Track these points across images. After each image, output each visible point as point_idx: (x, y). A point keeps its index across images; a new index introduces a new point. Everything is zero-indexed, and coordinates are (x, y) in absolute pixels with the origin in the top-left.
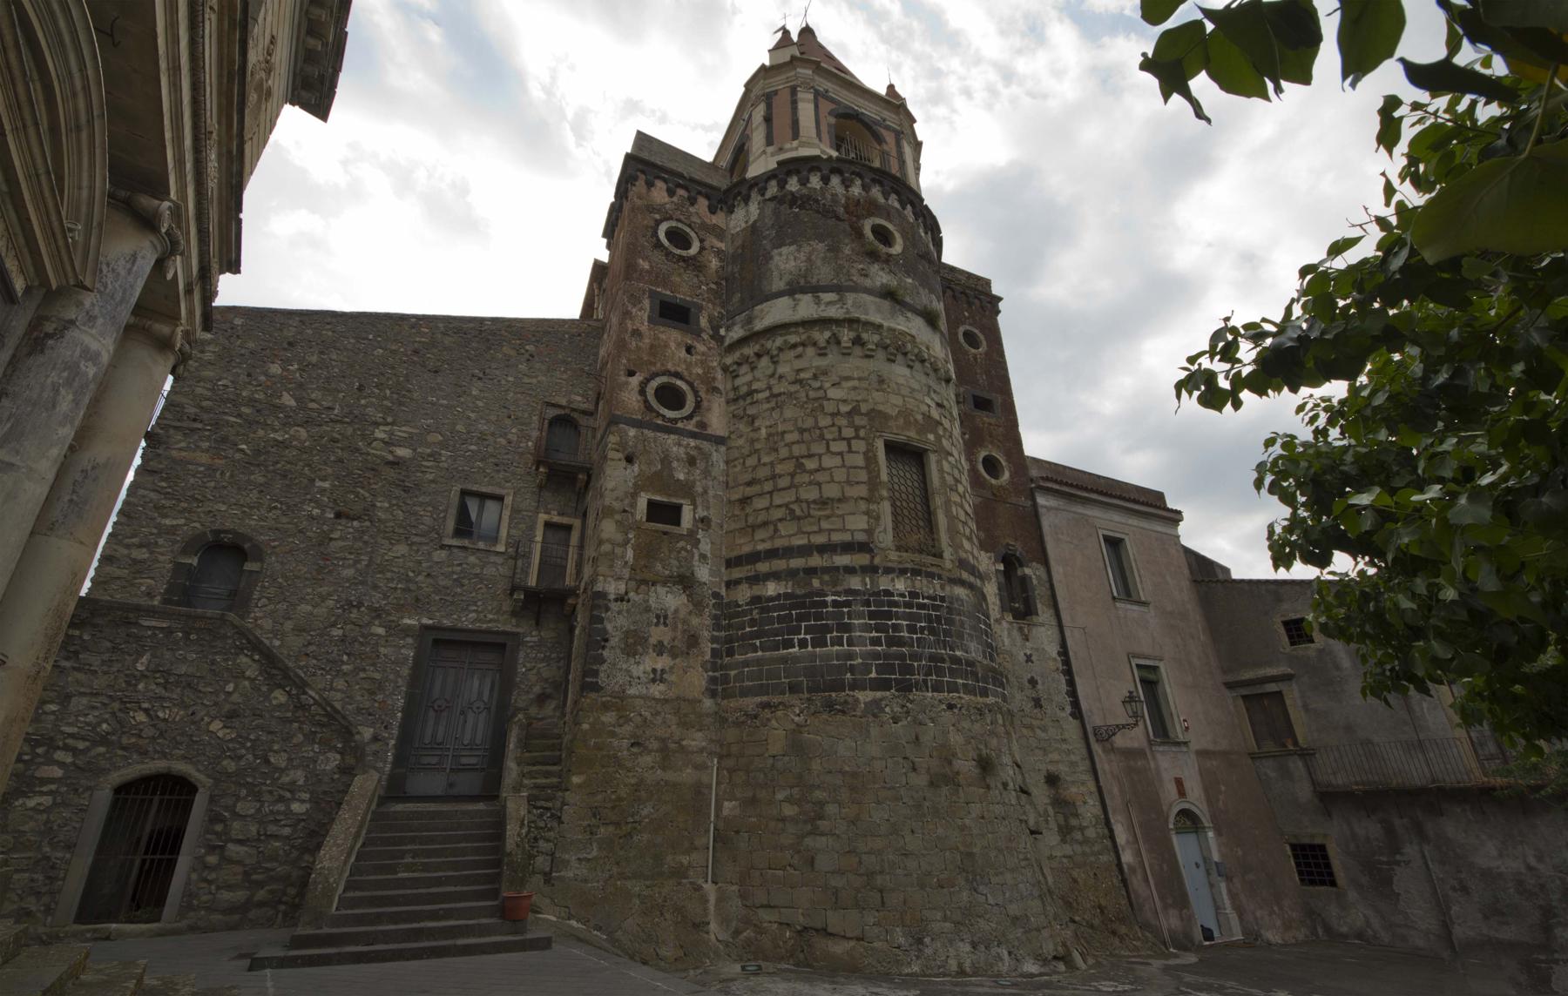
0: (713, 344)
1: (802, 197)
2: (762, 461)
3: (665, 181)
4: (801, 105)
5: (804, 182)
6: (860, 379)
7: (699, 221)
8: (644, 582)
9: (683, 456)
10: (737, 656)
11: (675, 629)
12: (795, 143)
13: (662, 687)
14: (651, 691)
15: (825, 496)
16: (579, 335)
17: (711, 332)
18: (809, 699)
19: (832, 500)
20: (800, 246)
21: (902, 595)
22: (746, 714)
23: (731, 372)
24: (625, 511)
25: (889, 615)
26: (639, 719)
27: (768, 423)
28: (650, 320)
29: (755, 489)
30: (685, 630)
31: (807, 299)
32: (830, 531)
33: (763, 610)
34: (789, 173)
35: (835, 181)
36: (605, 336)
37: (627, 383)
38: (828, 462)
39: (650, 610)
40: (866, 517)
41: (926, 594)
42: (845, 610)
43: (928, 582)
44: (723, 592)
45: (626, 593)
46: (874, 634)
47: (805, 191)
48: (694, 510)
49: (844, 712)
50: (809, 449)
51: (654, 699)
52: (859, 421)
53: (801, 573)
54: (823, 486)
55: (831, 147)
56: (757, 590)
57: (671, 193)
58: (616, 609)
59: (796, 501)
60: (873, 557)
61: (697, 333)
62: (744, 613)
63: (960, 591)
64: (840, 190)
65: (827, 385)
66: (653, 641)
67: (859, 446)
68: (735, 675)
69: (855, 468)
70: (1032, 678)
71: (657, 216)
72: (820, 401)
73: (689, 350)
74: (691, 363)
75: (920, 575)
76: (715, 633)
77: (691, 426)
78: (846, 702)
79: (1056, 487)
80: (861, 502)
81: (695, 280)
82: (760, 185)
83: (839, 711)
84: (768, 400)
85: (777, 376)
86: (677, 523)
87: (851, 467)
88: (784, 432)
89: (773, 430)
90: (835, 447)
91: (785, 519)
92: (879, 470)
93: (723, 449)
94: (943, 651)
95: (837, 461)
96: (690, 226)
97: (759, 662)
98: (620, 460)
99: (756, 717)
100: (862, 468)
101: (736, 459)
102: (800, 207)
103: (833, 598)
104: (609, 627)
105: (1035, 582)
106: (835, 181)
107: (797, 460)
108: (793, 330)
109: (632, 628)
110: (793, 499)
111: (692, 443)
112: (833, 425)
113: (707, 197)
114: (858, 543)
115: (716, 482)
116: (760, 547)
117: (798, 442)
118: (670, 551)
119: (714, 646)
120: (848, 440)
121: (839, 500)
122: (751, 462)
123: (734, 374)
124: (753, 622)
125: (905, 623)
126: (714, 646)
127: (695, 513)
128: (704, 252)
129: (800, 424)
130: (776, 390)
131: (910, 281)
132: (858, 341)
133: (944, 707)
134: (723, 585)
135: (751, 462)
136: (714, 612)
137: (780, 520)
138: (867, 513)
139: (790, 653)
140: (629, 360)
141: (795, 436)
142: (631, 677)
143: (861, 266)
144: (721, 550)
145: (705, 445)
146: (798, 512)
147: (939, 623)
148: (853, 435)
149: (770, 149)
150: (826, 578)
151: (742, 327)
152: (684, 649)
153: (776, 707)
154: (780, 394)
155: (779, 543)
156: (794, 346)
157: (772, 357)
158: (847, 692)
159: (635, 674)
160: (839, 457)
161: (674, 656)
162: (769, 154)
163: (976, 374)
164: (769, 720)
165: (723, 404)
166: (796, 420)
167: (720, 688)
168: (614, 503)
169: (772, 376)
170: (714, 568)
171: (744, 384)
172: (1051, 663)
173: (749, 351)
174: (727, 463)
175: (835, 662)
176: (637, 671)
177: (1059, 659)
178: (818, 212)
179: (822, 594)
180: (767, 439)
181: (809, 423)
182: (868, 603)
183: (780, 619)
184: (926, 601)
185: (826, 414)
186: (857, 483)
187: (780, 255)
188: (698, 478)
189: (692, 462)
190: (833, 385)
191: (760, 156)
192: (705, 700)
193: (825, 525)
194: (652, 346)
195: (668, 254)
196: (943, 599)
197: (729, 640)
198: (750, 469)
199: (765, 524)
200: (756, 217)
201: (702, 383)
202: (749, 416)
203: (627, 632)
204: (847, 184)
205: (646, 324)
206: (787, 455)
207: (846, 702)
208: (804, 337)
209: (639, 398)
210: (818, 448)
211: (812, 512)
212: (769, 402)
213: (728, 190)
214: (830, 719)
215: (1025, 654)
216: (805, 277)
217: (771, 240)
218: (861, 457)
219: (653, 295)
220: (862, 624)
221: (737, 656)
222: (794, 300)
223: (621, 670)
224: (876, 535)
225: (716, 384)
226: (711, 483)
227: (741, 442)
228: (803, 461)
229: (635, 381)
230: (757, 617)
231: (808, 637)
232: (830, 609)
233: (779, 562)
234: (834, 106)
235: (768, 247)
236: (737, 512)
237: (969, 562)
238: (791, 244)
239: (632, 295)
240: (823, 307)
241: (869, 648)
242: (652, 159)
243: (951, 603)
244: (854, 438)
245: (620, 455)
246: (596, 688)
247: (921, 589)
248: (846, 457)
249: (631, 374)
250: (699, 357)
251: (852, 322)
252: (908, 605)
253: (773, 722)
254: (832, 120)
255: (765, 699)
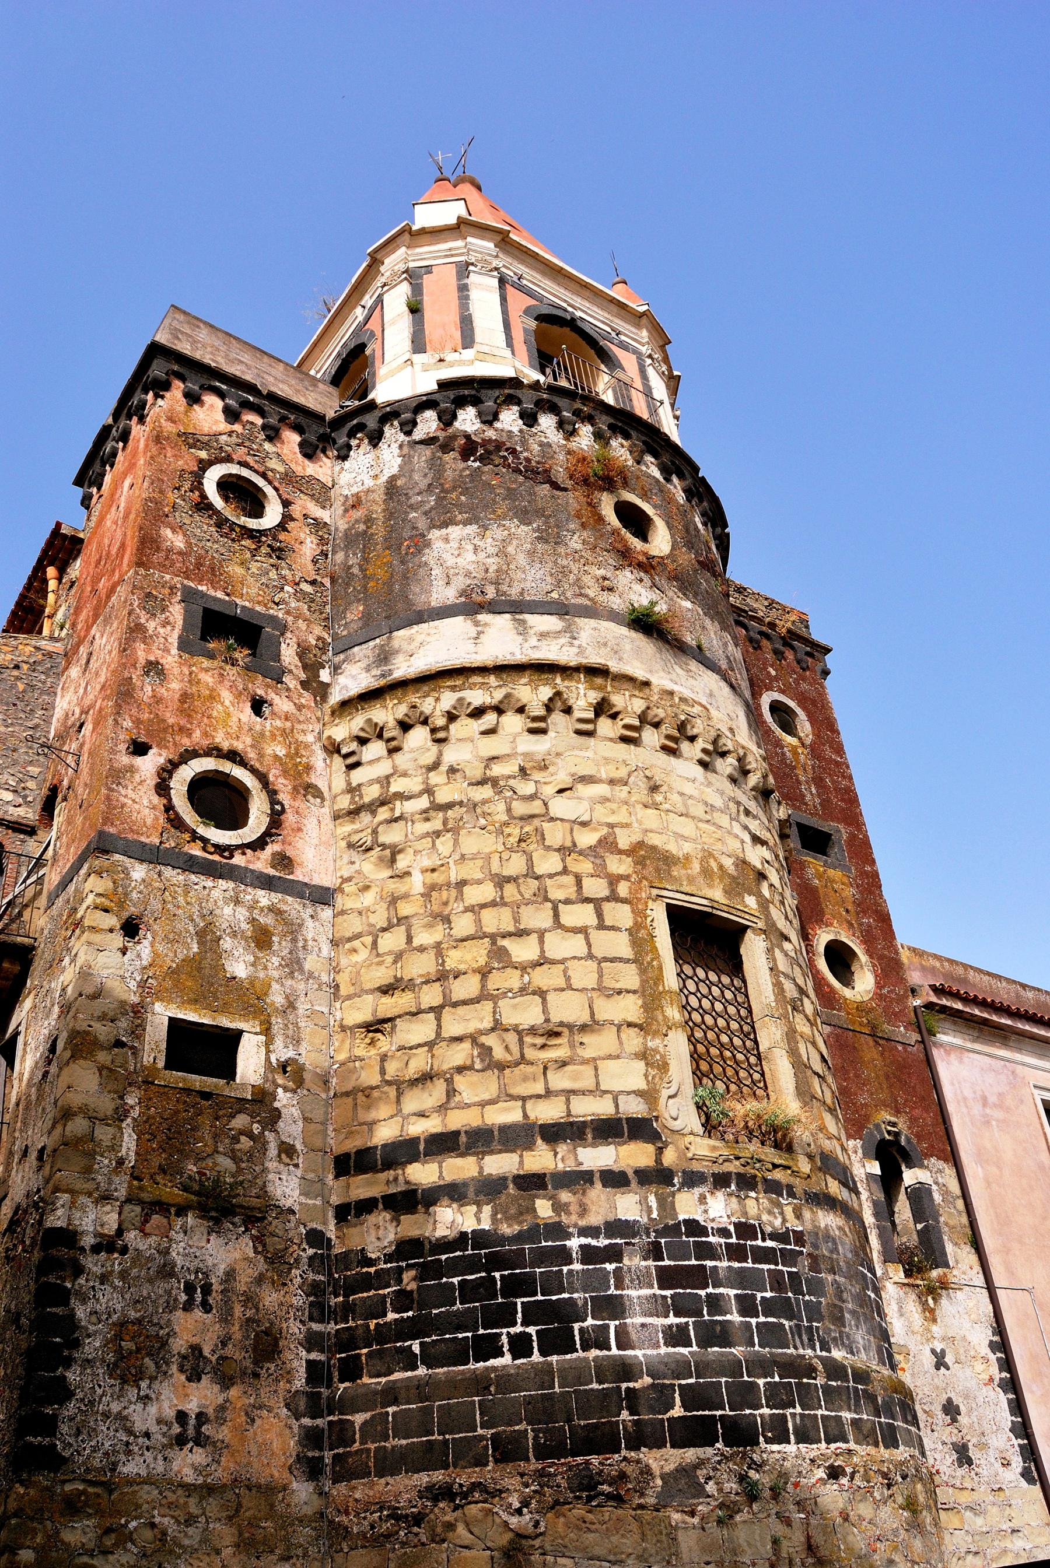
0: (307, 699)
1: (486, 442)
2: (416, 942)
3: (222, 395)
4: (474, 294)
5: (490, 419)
6: (612, 782)
7: (281, 469)
8: (160, 1206)
9: (244, 926)
10: (366, 1380)
11: (226, 1318)
12: (468, 354)
13: (199, 1456)
14: (175, 1466)
15: (555, 1018)
16: (17, 667)
17: (303, 676)
18: (541, 1474)
19: (570, 1027)
20: (486, 528)
21: (724, 1232)
22: (395, 1516)
23: (346, 756)
24: (119, 1044)
25: (699, 1277)
26: (148, 1534)
27: (427, 863)
28: (184, 645)
29: (401, 1002)
30: (249, 1320)
31: (500, 624)
32: (569, 1093)
33: (426, 1272)
34: (461, 402)
35: (547, 422)
36: (74, 672)
37: (131, 769)
38: (559, 946)
39: (172, 1274)
40: (641, 1065)
41: (768, 1229)
42: (610, 1267)
43: (771, 1201)
44: (331, 1231)
45: (120, 1232)
46: (672, 1320)
47: (491, 434)
48: (268, 1044)
49: (618, 1500)
50: (517, 920)
51: (183, 1485)
52: (618, 865)
53: (512, 1189)
54: (550, 997)
55: (532, 366)
56: (411, 1226)
57: (232, 415)
58: (97, 1270)
59: (493, 1029)
60: (660, 1151)
61: (277, 677)
62: (381, 1279)
63: (829, 1220)
64: (555, 437)
65: (549, 791)
66: (179, 1345)
67: (621, 915)
68: (365, 1423)
69: (612, 960)
70: (949, 1401)
71: (203, 454)
72: (536, 822)
73: (258, 706)
74: (262, 734)
75: (753, 1187)
76: (316, 1327)
77: (261, 862)
78: (623, 1476)
79: (959, 1006)
80: (633, 1032)
81: (273, 574)
82: (404, 416)
83: (609, 1497)
84: (426, 815)
85: (444, 768)
86: (228, 1070)
87: (606, 959)
88: (462, 884)
89: (437, 878)
90: (572, 915)
91: (470, 1068)
92: (660, 968)
93: (326, 913)
94: (809, 1352)
95: (576, 945)
96: (264, 475)
97: (421, 1390)
98: (111, 931)
99: (418, 1520)
100: (627, 961)
101: (357, 936)
102: (481, 459)
103: (584, 1241)
104: (81, 1313)
105: (937, 1197)
106: (547, 422)
107: (494, 943)
108: (476, 679)
109: (133, 1315)
110: (487, 1024)
111: (264, 898)
112: (565, 871)
113: (298, 429)
114: (629, 1120)
115: (312, 984)
116: (418, 1128)
117: (493, 904)
118: (215, 1136)
119: (314, 1356)
120: (597, 903)
121: (584, 1028)
122: (393, 941)
123: (351, 760)
124: (402, 1301)
125: (732, 1292)
126: (314, 1356)
127: (268, 1052)
128: (291, 525)
129: (495, 867)
130: (443, 796)
131: (688, 604)
132: (602, 708)
133: (821, 1473)
134: (331, 1214)
135: (393, 941)
136: (311, 1276)
137: (460, 1070)
138: (644, 1055)
139: (494, 1369)
140: (137, 722)
141: (487, 892)
142: (130, 1432)
143: (602, 572)
144: (325, 1135)
145: (291, 905)
146: (499, 1053)
147: (798, 1291)
148: (605, 892)
149: (418, 358)
150: (565, 1196)
151: (368, 669)
152: (248, 1363)
153: (465, 1496)
154: (450, 806)
155: (458, 1120)
156: (478, 713)
157: (433, 731)
158: (624, 1452)
159: (139, 1426)
160: (581, 937)
161: (226, 1382)
162: (418, 367)
163: (799, 782)
164: (450, 1526)
165: (327, 820)
166: (488, 858)
167: (328, 1456)
168: (97, 1026)
169: (435, 766)
170: (311, 1176)
171: (371, 782)
172: (979, 1367)
173: (386, 714)
174: (335, 943)
175: (595, 1386)
176: (144, 1418)
177: (993, 1358)
178: (517, 471)
179: (558, 1230)
180: (427, 895)
181: (516, 865)
182: (654, 1250)
183: (446, 1295)
184: (770, 1244)
185: (548, 848)
186: (619, 993)
187: (447, 540)
188: (276, 974)
189: (262, 939)
190: (561, 791)
191: (400, 369)
192: (295, 1485)
193: (559, 1080)
194: (185, 697)
195: (221, 522)
196: (799, 1238)
197: (347, 1341)
198: (389, 959)
199: (426, 1078)
200: (395, 470)
201: (285, 773)
202: (384, 846)
203: (122, 1324)
204: (567, 429)
205: (174, 651)
206: (471, 930)
207: (623, 1476)
208: (498, 695)
209: (156, 799)
210: (538, 918)
211: (530, 1054)
212: (427, 819)
213: (338, 423)
214: (590, 1516)
215: (933, 1351)
216: (497, 583)
217: (425, 513)
218: (624, 938)
219: (189, 597)
220: (648, 1298)
221: (366, 1380)
222: (477, 624)
223: (106, 1415)
224: (662, 1101)
225: (313, 779)
226: (301, 986)
227: (369, 899)
228: (505, 943)
229: (149, 764)
230: (412, 1286)
231: (532, 1330)
232: (577, 1266)
233: (459, 1161)
234: (533, 302)
235: (422, 524)
236: (359, 1052)
237: (837, 1158)
238: (466, 523)
239: (149, 595)
240: (533, 641)
241: (663, 1350)
242: (197, 355)
243: (815, 1246)
244: (607, 899)
245: (112, 921)
246: (53, 1461)
247: (759, 1218)
248: (595, 935)
249: (140, 749)
250: (278, 723)
251: (594, 672)
252: (736, 1253)
253: (461, 1529)
254: (533, 324)
255: (438, 1476)
